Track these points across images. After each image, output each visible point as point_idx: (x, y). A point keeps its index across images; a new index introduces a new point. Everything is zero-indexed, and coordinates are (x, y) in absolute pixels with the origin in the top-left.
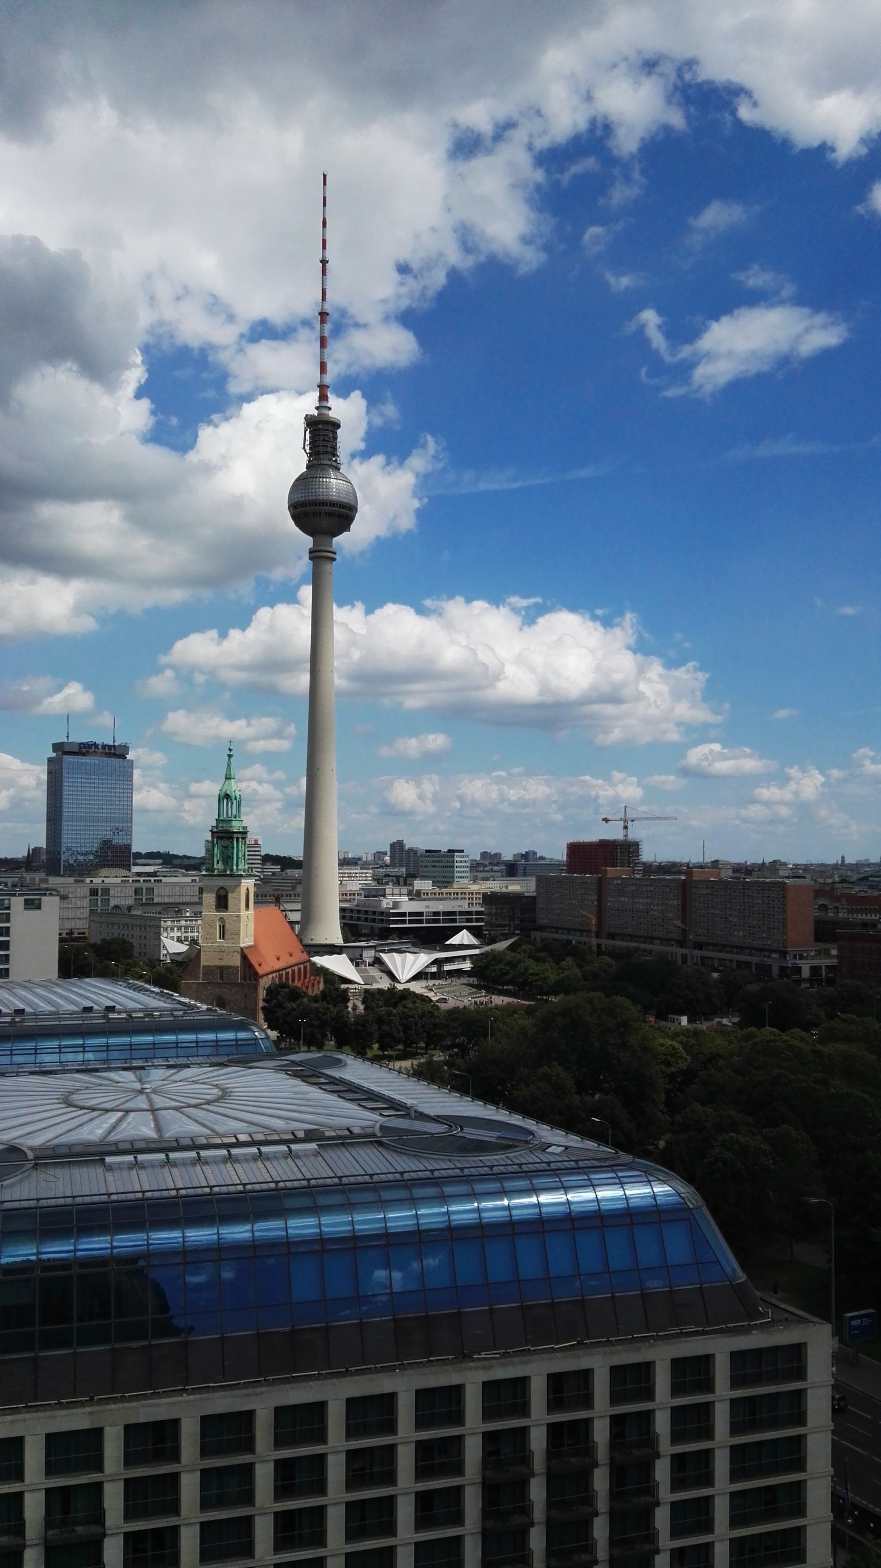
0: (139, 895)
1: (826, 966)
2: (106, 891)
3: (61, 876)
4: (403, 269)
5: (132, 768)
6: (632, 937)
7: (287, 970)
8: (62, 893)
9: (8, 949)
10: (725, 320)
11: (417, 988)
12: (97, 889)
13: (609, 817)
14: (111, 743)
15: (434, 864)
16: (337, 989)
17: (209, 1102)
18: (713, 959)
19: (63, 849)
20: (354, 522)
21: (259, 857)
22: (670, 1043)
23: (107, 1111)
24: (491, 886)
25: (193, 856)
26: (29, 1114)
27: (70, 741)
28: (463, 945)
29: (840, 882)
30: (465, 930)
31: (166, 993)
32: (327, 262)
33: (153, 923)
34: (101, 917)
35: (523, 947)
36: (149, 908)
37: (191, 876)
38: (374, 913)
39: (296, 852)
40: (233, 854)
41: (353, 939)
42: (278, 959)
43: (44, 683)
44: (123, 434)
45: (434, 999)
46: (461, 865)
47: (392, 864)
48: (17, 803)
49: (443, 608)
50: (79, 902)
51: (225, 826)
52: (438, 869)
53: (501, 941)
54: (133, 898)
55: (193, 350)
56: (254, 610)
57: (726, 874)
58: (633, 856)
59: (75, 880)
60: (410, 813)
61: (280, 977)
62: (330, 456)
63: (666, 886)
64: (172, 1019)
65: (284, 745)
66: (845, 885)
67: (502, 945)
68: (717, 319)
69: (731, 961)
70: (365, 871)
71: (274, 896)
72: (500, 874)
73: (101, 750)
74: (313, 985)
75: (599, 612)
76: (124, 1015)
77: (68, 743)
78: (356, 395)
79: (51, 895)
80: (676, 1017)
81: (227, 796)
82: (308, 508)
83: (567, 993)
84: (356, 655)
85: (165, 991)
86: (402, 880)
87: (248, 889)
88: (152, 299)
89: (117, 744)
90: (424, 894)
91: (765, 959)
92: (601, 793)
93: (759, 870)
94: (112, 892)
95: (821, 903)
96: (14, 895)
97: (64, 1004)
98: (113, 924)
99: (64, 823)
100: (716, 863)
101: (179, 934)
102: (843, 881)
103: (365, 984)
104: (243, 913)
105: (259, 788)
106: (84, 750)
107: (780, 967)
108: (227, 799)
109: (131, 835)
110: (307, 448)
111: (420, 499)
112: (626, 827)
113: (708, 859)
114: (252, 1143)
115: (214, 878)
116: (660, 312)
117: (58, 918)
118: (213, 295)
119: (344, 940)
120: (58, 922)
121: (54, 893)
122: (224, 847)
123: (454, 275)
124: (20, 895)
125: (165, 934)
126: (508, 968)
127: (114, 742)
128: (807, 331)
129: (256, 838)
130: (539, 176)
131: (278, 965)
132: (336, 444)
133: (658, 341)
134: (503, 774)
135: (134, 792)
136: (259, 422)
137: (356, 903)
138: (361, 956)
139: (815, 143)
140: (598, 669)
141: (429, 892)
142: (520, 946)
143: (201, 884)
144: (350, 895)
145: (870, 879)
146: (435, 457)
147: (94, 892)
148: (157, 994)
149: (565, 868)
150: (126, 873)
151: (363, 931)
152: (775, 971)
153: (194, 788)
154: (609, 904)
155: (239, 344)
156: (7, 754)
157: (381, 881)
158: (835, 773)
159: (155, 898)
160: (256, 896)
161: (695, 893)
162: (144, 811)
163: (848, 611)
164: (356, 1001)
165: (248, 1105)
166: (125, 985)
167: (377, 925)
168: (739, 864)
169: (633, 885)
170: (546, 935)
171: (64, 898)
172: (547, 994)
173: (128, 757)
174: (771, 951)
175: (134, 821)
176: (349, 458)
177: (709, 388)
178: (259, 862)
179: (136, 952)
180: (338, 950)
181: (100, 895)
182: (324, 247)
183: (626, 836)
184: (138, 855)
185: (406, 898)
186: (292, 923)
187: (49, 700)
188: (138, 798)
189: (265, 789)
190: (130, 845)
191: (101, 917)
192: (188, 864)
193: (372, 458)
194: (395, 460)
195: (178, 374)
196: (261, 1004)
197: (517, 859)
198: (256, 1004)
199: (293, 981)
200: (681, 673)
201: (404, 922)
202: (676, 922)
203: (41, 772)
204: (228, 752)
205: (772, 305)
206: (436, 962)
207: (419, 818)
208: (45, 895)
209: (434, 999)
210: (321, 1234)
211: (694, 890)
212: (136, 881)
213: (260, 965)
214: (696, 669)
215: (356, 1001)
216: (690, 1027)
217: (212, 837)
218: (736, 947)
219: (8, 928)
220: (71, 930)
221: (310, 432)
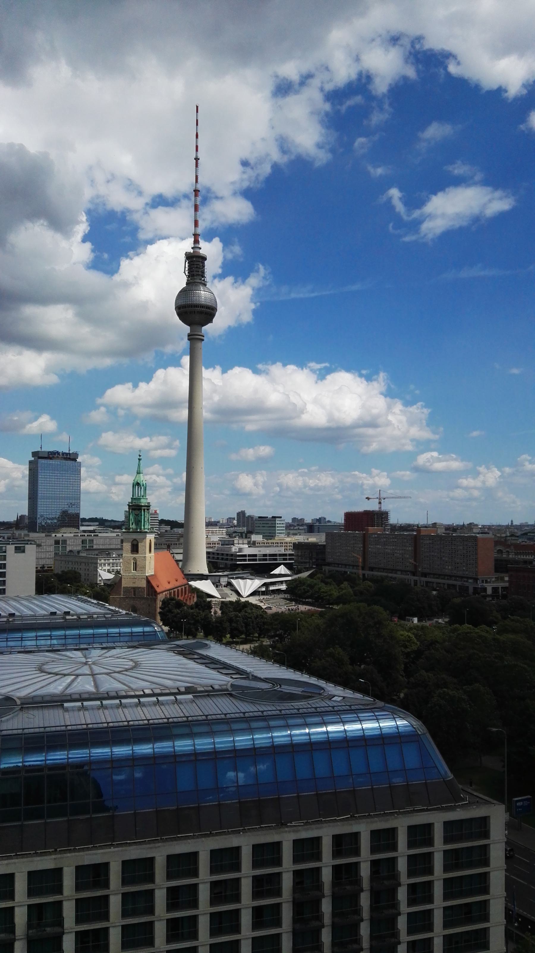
0: (84, 544)
1: (501, 587)
2: (65, 542)
3: (37, 532)
4: (245, 163)
5: (80, 467)
6: (384, 570)
7: (174, 590)
8: (38, 543)
9: (5, 577)
10: (440, 194)
11: (253, 600)
12: (59, 540)
13: (370, 497)
14: (68, 452)
15: (264, 525)
16: (205, 601)
17: (127, 670)
18: (433, 583)
19: (39, 516)
20: (215, 317)
21: (158, 521)
22: (407, 634)
23: (65, 675)
24: (298, 538)
25: (117, 520)
26: (18, 677)
27: (42, 450)
28: (281, 574)
29: (510, 536)
30: (282, 565)
31: (101, 604)
32: (199, 159)
33: (93, 561)
34: (61, 557)
35: (318, 576)
36: (90, 552)
37: (116, 532)
38: (227, 555)
39: (180, 518)
40: (141, 519)
41: (214, 571)
42: (169, 583)
43: (26, 415)
44: (74, 264)
45: (264, 607)
46: (280, 525)
47: (238, 525)
48: (10, 488)
49: (269, 370)
50: (48, 548)
51: (137, 502)
52: (266, 528)
53: (304, 572)
54: (81, 546)
55: (117, 212)
56: (154, 371)
57: (441, 531)
58: (384, 520)
59: (46, 535)
60: (249, 494)
61: (170, 594)
62: (200, 277)
63: (405, 538)
64: (104, 619)
65: (172, 453)
66: (513, 538)
67: (305, 575)
68: (435, 194)
69: (444, 584)
70: (221, 529)
71: (166, 545)
72: (303, 531)
73: (61, 456)
74: (190, 599)
75: (364, 372)
76: (75, 617)
77: (41, 452)
78: (216, 240)
79: (31, 544)
80: (410, 618)
81: (138, 484)
82: (187, 309)
83: (344, 603)
84: (216, 398)
85: (100, 602)
86: (244, 535)
87: (150, 540)
88: (92, 182)
89: (71, 452)
90: (257, 543)
91: (464, 583)
92: (365, 482)
93: (461, 529)
94: (68, 542)
95: (498, 549)
96: (9, 544)
97: (39, 610)
98: (68, 562)
99: (39, 500)
100: (435, 525)
101: (109, 568)
102: (512, 535)
103: (222, 598)
104: (148, 555)
105: (158, 479)
106: (51, 456)
107: (474, 588)
108: (138, 485)
109: (80, 507)
110: (187, 272)
111: (255, 303)
112: (380, 503)
113: (430, 522)
114: (153, 695)
115: (130, 534)
116: (401, 190)
117: (35, 558)
118: (130, 180)
119: (209, 572)
120: (35, 560)
121: (33, 543)
122: (136, 515)
123: (275, 167)
124: (12, 544)
125: (100, 568)
126: (309, 589)
127: (69, 451)
128: (490, 201)
129: (156, 509)
130: (327, 107)
131: (169, 587)
132: (204, 270)
133: (400, 207)
134: (306, 470)
135: (81, 481)
136: (158, 256)
137: (216, 549)
138: (219, 581)
139: (495, 87)
140: (363, 406)
141: (261, 542)
142: (316, 575)
143: (122, 537)
144: (213, 544)
145: (529, 534)
146: (264, 278)
147: (57, 542)
148: (95, 604)
149: (343, 527)
150: (77, 530)
151: (221, 566)
152: (471, 590)
153: (118, 479)
154: (370, 549)
155: (145, 209)
156: (4, 458)
157: (231, 536)
158: (507, 470)
159: (94, 546)
160: (156, 544)
161: (422, 543)
162: (88, 493)
163: (515, 371)
164: (216, 609)
165: (151, 672)
166: (76, 598)
167: (229, 562)
168: (448, 525)
169: (384, 538)
170: (332, 568)
171: (39, 546)
172: (332, 604)
173: (78, 460)
174: (468, 578)
175: (81, 499)
176: (212, 278)
177: (430, 236)
178: (157, 524)
179: (82, 579)
180: (205, 577)
181: (60, 544)
182: (197, 150)
183: (380, 508)
184: (84, 520)
185: (247, 546)
186: (177, 561)
187: (30, 425)
188: (84, 485)
189: (161, 480)
190: (79, 514)
191: (61, 557)
192: (114, 525)
193: (226, 279)
194: (240, 280)
195: (108, 227)
196: (159, 610)
197: (314, 522)
198: (156, 610)
199: (178, 596)
200: (414, 409)
201: (245, 560)
202: (411, 561)
203: (25, 469)
204: (139, 457)
205: (469, 186)
206: (265, 585)
207: (254, 497)
208: (27, 544)
209: (264, 607)
210: (195, 750)
211: (421, 541)
212: (83, 535)
213: (158, 586)
214: (422, 407)
215: (216, 609)
216: (419, 624)
217: (129, 509)
218: (447, 576)
219: (5, 564)
220: (43, 565)
221: (188, 263)
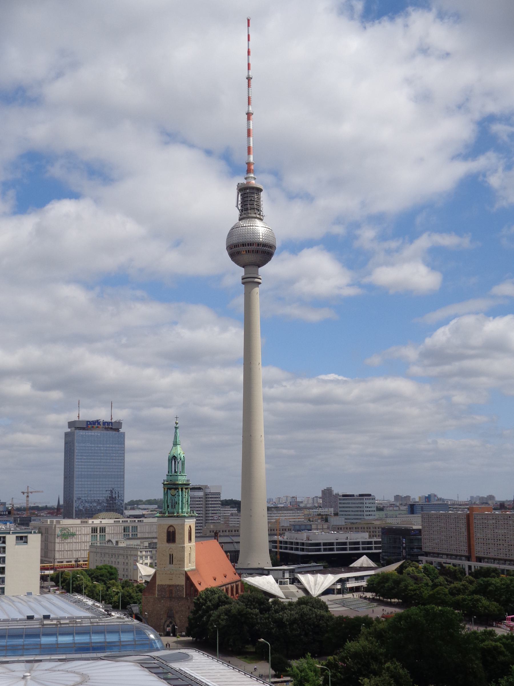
2: (103, 530)
7: (227, 586)
12: (97, 528)
14: (110, 421)
19: (75, 499)
21: (219, 502)
30: (365, 556)
33: (132, 553)
40: (179, 500)
54: (123, 534)
64: (89, 624)
67: (393, 568)
71: (213, 532)
73: (102, 426)
76: (55, 622)
77: (79, 421)
81: (174, 458)
87: (190, 527)
89: (113, 421)
94: (107, 530)
99: (75, 479)
104: (187, 544)
108: (174, 459)
110: (240, 207)
115: (164, 518)
122: (172, 495)
124: (13, 533)
125: (141, 561)
127: (111, 420)
135: (126, 454)
141: (342, 527)
147: (94, 530)
173: (121, 430)
180: (266, 572)
206: (341, 581)
208: (31, 533)
212: (125, 521)
213: (200, 584)
221: (241, 195)
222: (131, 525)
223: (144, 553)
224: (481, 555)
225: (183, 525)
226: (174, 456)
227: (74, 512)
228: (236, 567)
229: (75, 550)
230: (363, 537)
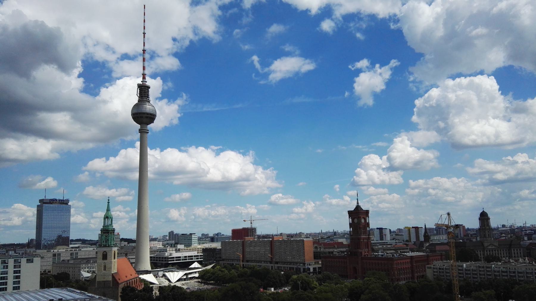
0: (72, 256)
1: (318, 267)
2: (59, 255)
3: (42, 249)
4: (174, 40)
5: (70, 208)
6: (255, 261)
7: (135, 279)
8: (42, 256)
10: (278, 60)
11: (179, 284)
12: (56, 254)
13: (245, 220)
14: (63, 199)
15: (185, 239)
16: (149, 287)
18: (281, 267)
20: (155, 120)
21: (119, 239)
22: (268, 298)
24: (205, 246)
28: (195, 267)
29: (321, 239)
30: (196, 262)
31: (82, 292)
34: (57, 265)
35: (217, 267)
36: (76, 261)
37: (93, 247)
38: (163, 258)
39: (134, 237)
40: (109, 238)
41: (155, 268)
42: (131, 275)
43: (38, 177)
44: (73, 89)
45: (185, 288)
46: (195, 238)
47: (170, 240)
48: (25, 222)
49: (188, 150)
52: (186, 240)
53: (209, 265)
55: (100, 62)
56: (119, 151)
57: (285, 238)
58: (254, 233)
59: (47, 251)
60: (177, 221)
61: (127, 283)
63: (265, 243)
65: (131, 198)
66: (322, 240)
67: (209, 267)
68: (276, 60)
69: (287, 267)
70: (159, 243)
71: (125, 253)
72: (208, 241)
74: (140, 286)
75: (241, 151)
78: (159, 78)
79: (37, 257)
80: (270, 288)
83: (232, 282)
84: (157, 166)
85: (82, 292)
86: (173, 245)
87: (115, 251)
88: (85, 45)
89: (64, 199)
90: (181, 250)
91: (298, 266)
92: (243, 211)
93: (295, 236)
94: (61, 255)
95: (315, 246)
97: (42, 299)
100: (281, 234)
101: (88, 270)
102: (322, 238)
104: (113, 260)
105: (120, 214)
106: (51, 202)
107: (303, 268)
108: (107, 218)
109: (69, 233)
111: (180, 114)
112: (251, 223)
113: (279, 233)
116: (259, 57)
117: (40, 265)
118: (107, 45)
119: (151, 269)
120: (40, 267)
121: (38, 256)
123: (191, 42)
125: (82, 270)
126: (212, 275)
128: (303, 65)
130: (220, 13)
133: (258, 65)
134: (210, 206)
135: (71, 217)
136: (123, 86)
137: (156, 254)
138: (158, 274)
139: (304, 9)
140: (241, 170)
142: (216, 267)
143: (97, 250)
146: (186, 100)
147: (54, 255)
148: (79, 293)
149: (231, 238)
150: (67, 247)
151: (159, 265)
152: (302, 270)
153: (95, 214)
154: (246, 250)
155: (117, 61)
156: (22, 204)
157: (165, 246)
158: (318, 203)
160: (118, 254)
161: (275, 245)
162: (75, 224)
163: (319, 151)
164: (156, 291)
166: (66, 290)
167: (164, 262)
168: (289, 234)
169: (254, 243)
170: (225, 262)
171: (42, 258)
172: (226, 283)
173: (69, 204)
174: (300, 263)
175: (70, 228)
177: (274, 81)
178: (119, 241)
179: (71, 278)
181: (56, 256)
183: (252, 226)
184: (72, 240)
185: (174, 252)
186: (131, 263)
187: (40, 184)
188: (72, 219)
189: (122, 214)
190: (69, 237)
192: (91, 243)
193: (163, 100)
194: (172, 100)
195: (94, 70)
196: (120, 294)
197: (214, 236)
198: (118, 295)
199: (132, 285)
200: (268, 171)
201: (174, 260)
202: (269, 255)
203: (35, 210)
205: (293, 56)
206: (186, 274)
207: (180, 222)
208: (35, 257)
209: (185, 288)
211: (275, 244)
212: (71, 250)
214: (273, 170)
215: (156, 291)
216: (275, 291)
217: (101, 233)
220: (45, 270)
221: (139, 90)
222: (74, 252)
223: (84, 266)
224: (278, 260)
225: (111, 250)
226: (107, 217)
227: (42, 246)
228: (136, 270)
229: (44, 266)
230: (195, 253)
